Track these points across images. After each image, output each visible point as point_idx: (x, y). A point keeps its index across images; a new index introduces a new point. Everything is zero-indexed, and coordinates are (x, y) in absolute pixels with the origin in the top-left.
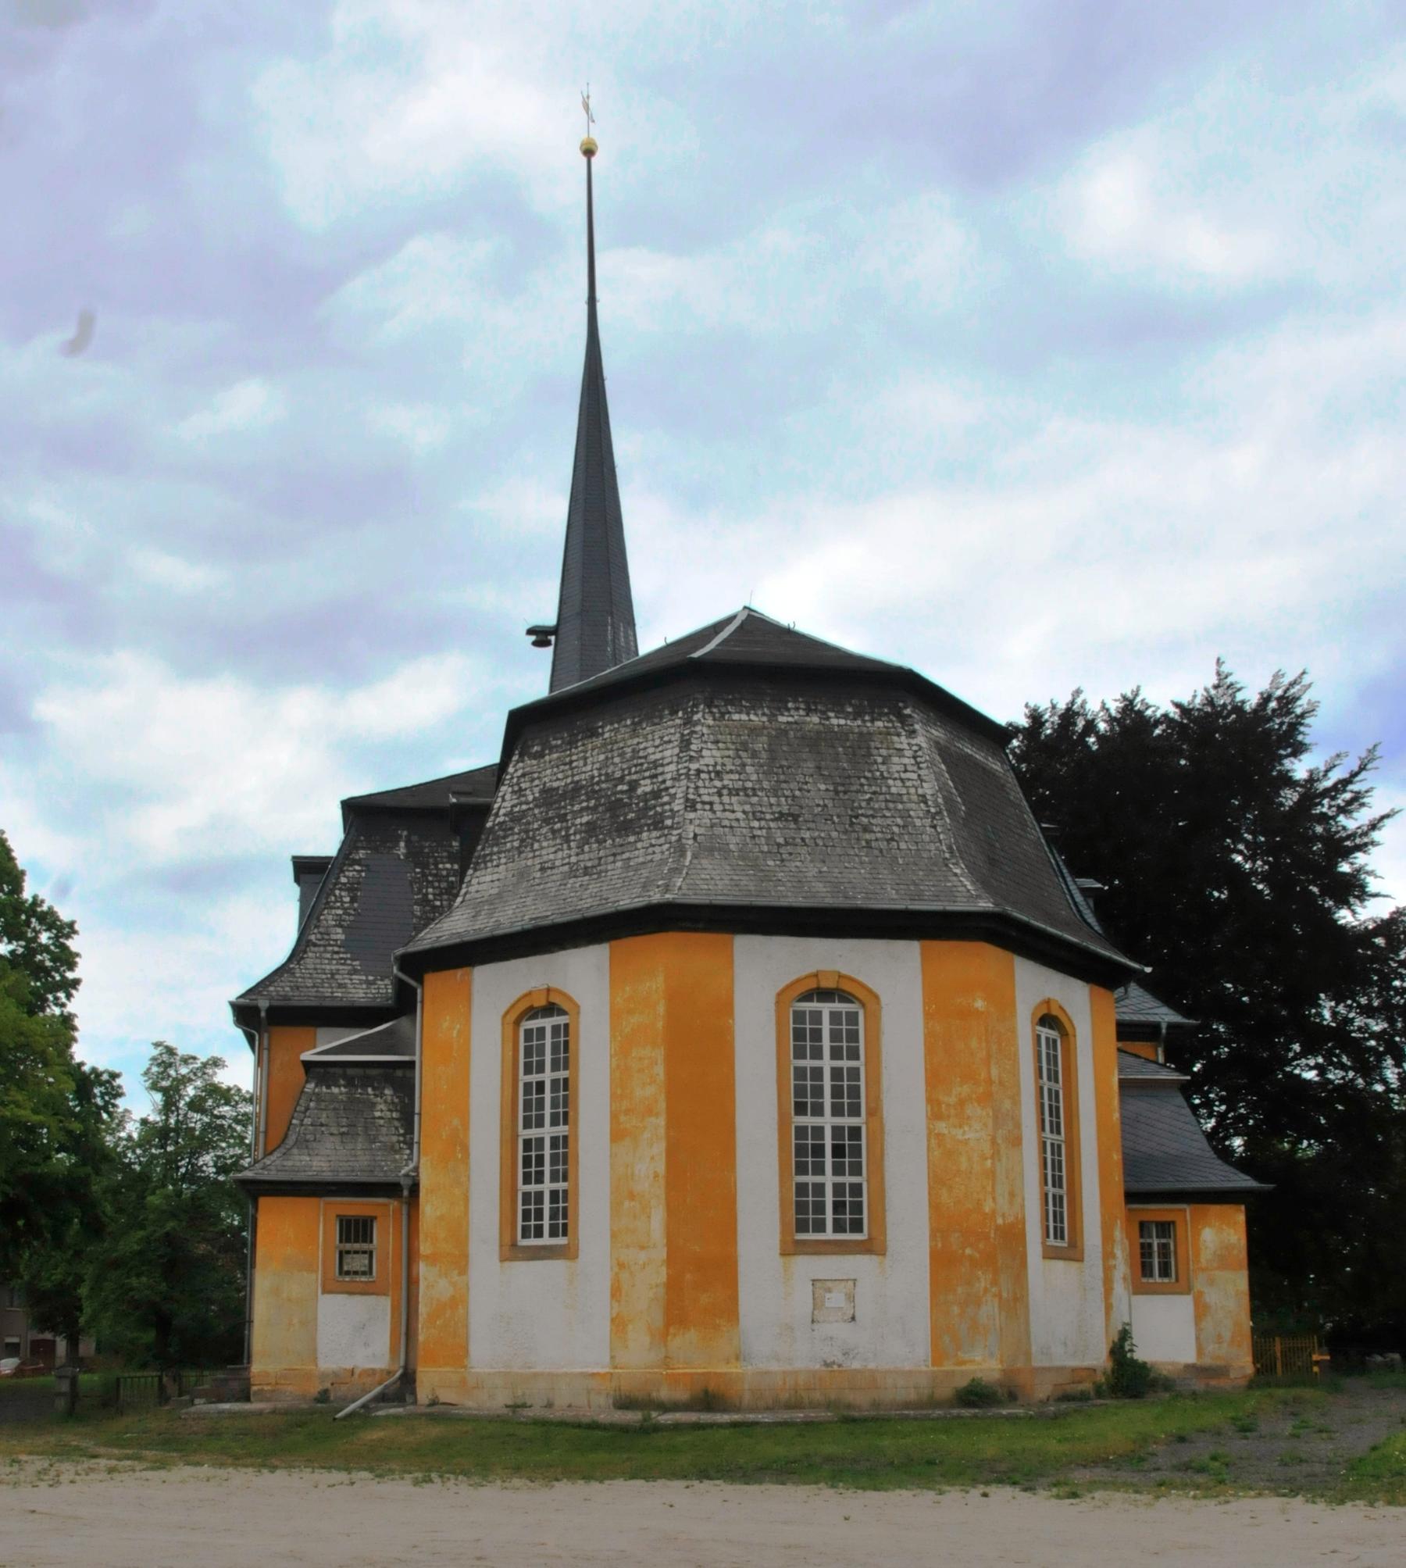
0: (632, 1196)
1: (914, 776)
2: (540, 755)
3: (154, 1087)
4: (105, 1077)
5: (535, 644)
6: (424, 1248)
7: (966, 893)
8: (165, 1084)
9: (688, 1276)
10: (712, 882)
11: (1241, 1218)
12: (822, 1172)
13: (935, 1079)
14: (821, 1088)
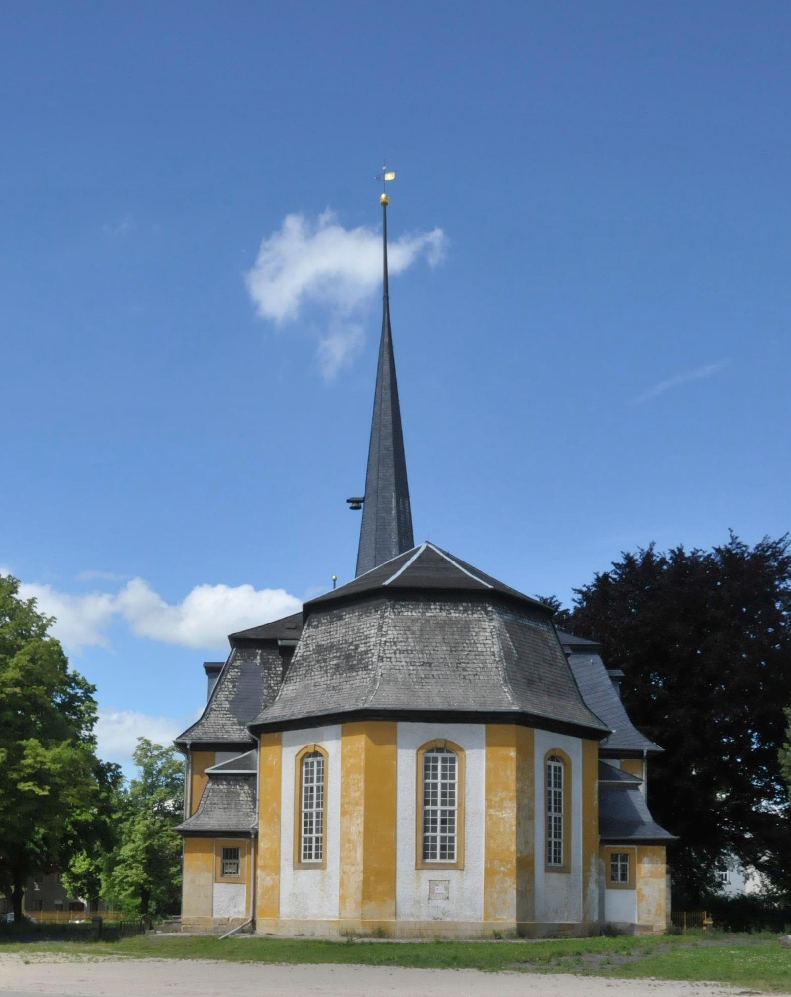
0: (349, 842)
1: (490, 642)
2: (317, 627)
3: (140, 763)
4: (113, 767)
5: (352, 508)
6: (260, 862)
7: (508, 702)
8: (146, 761)
9: (372, 878)
10: (388, 698)
11: (664, 853)
13: (489, 789)
14: (437, 793)
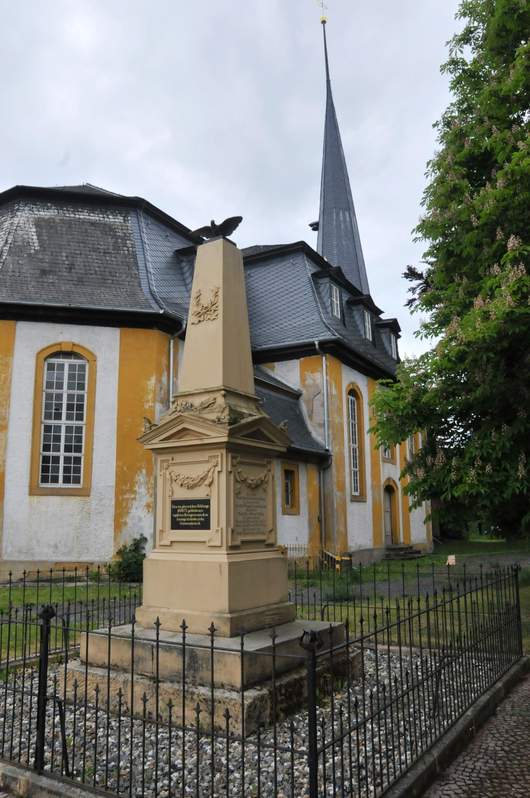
12: (58, 450)
14: (68, 409)
